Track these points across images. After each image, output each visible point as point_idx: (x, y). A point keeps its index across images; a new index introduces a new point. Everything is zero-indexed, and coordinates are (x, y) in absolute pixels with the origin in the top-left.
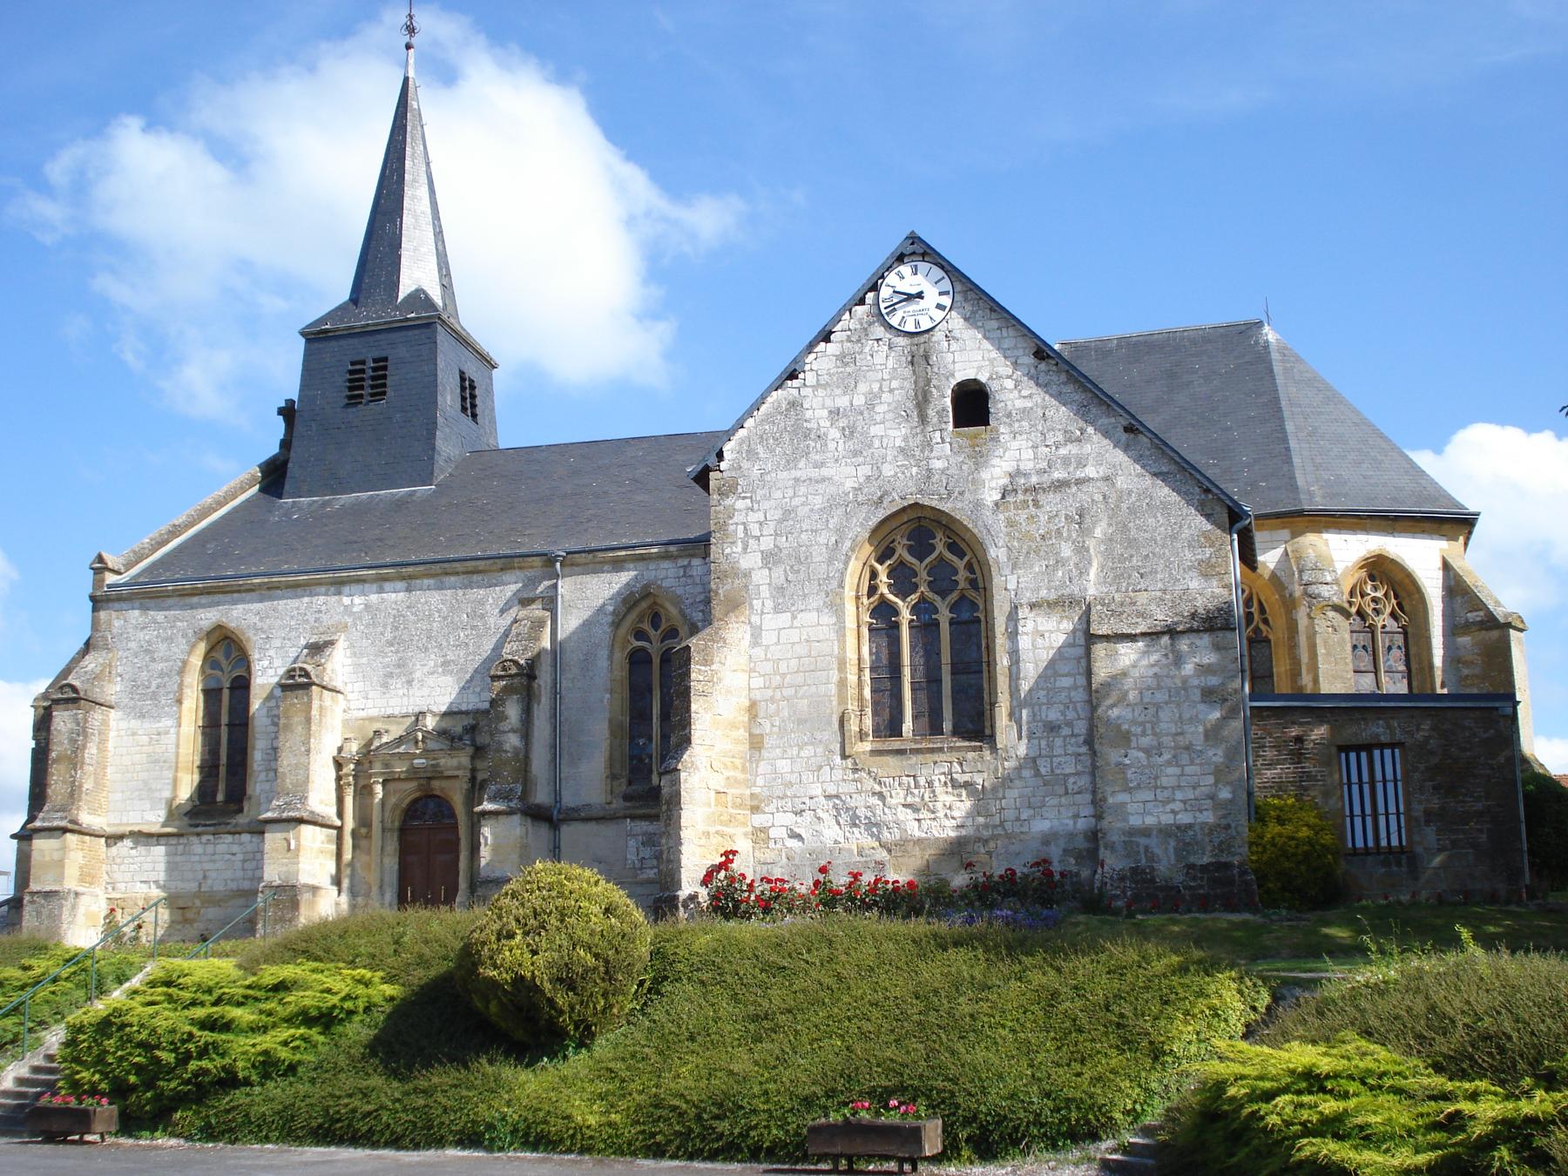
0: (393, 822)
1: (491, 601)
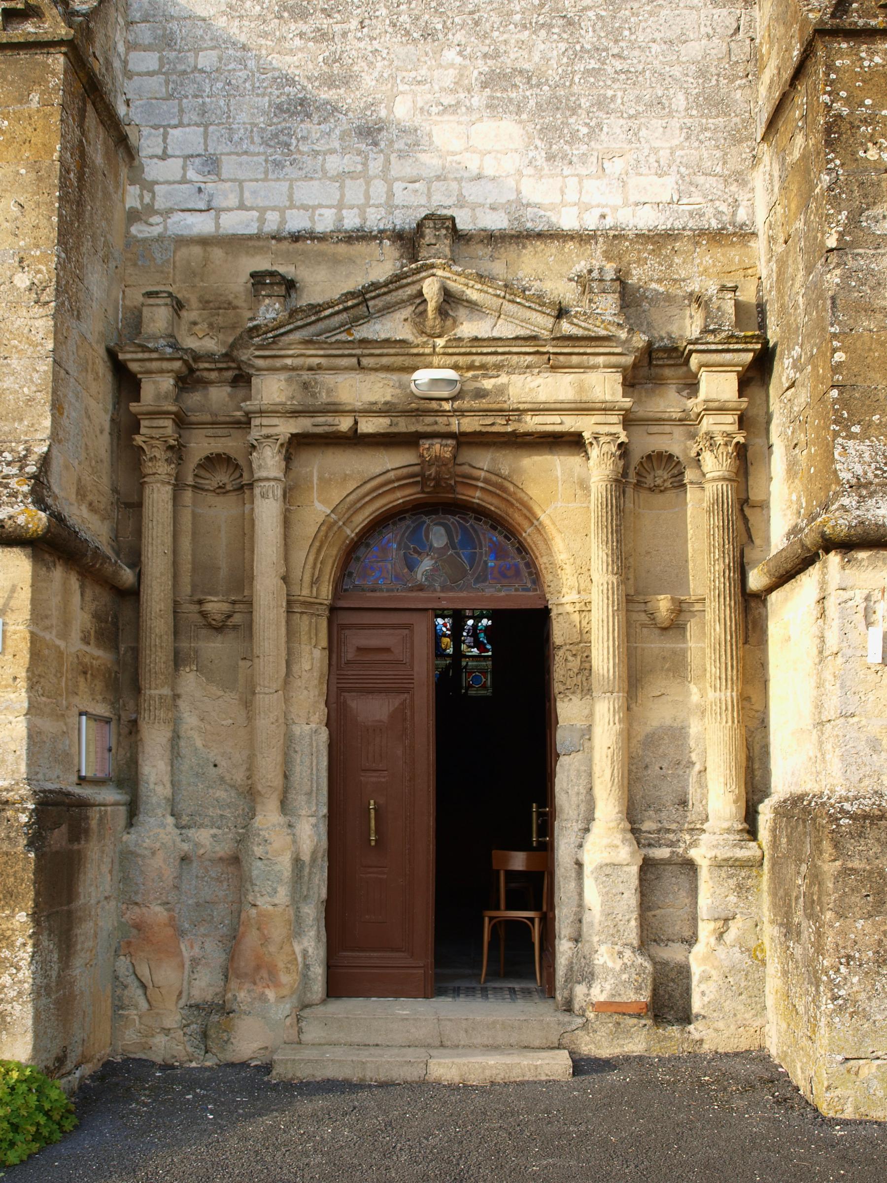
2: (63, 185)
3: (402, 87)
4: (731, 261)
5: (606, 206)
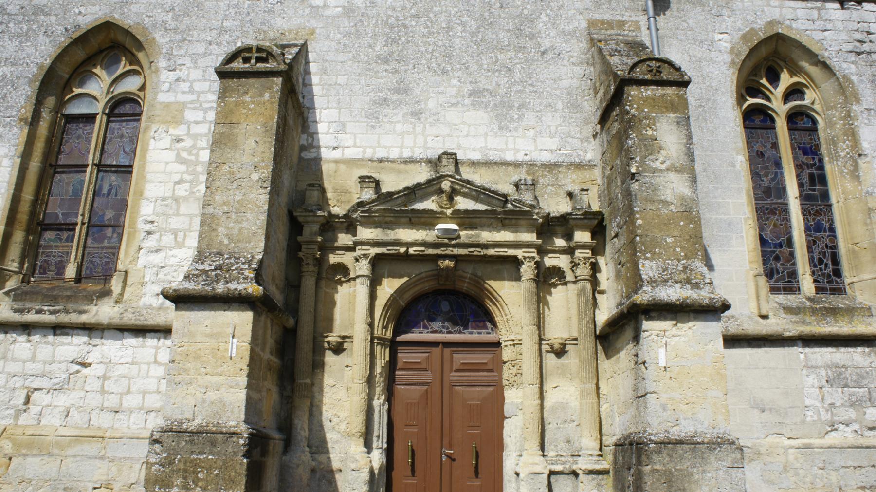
0: (385, 327)
1: (544, 18)
2: (277, 134)
3: (432, 95)
4: (586, 177)
5: (527, 150)
